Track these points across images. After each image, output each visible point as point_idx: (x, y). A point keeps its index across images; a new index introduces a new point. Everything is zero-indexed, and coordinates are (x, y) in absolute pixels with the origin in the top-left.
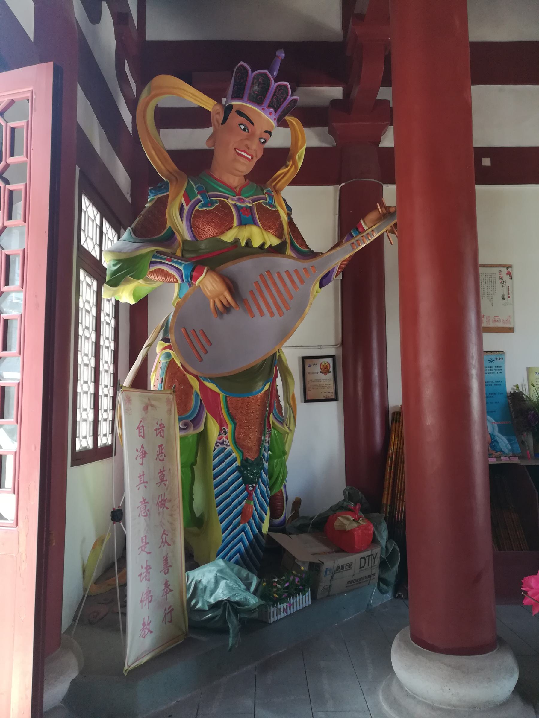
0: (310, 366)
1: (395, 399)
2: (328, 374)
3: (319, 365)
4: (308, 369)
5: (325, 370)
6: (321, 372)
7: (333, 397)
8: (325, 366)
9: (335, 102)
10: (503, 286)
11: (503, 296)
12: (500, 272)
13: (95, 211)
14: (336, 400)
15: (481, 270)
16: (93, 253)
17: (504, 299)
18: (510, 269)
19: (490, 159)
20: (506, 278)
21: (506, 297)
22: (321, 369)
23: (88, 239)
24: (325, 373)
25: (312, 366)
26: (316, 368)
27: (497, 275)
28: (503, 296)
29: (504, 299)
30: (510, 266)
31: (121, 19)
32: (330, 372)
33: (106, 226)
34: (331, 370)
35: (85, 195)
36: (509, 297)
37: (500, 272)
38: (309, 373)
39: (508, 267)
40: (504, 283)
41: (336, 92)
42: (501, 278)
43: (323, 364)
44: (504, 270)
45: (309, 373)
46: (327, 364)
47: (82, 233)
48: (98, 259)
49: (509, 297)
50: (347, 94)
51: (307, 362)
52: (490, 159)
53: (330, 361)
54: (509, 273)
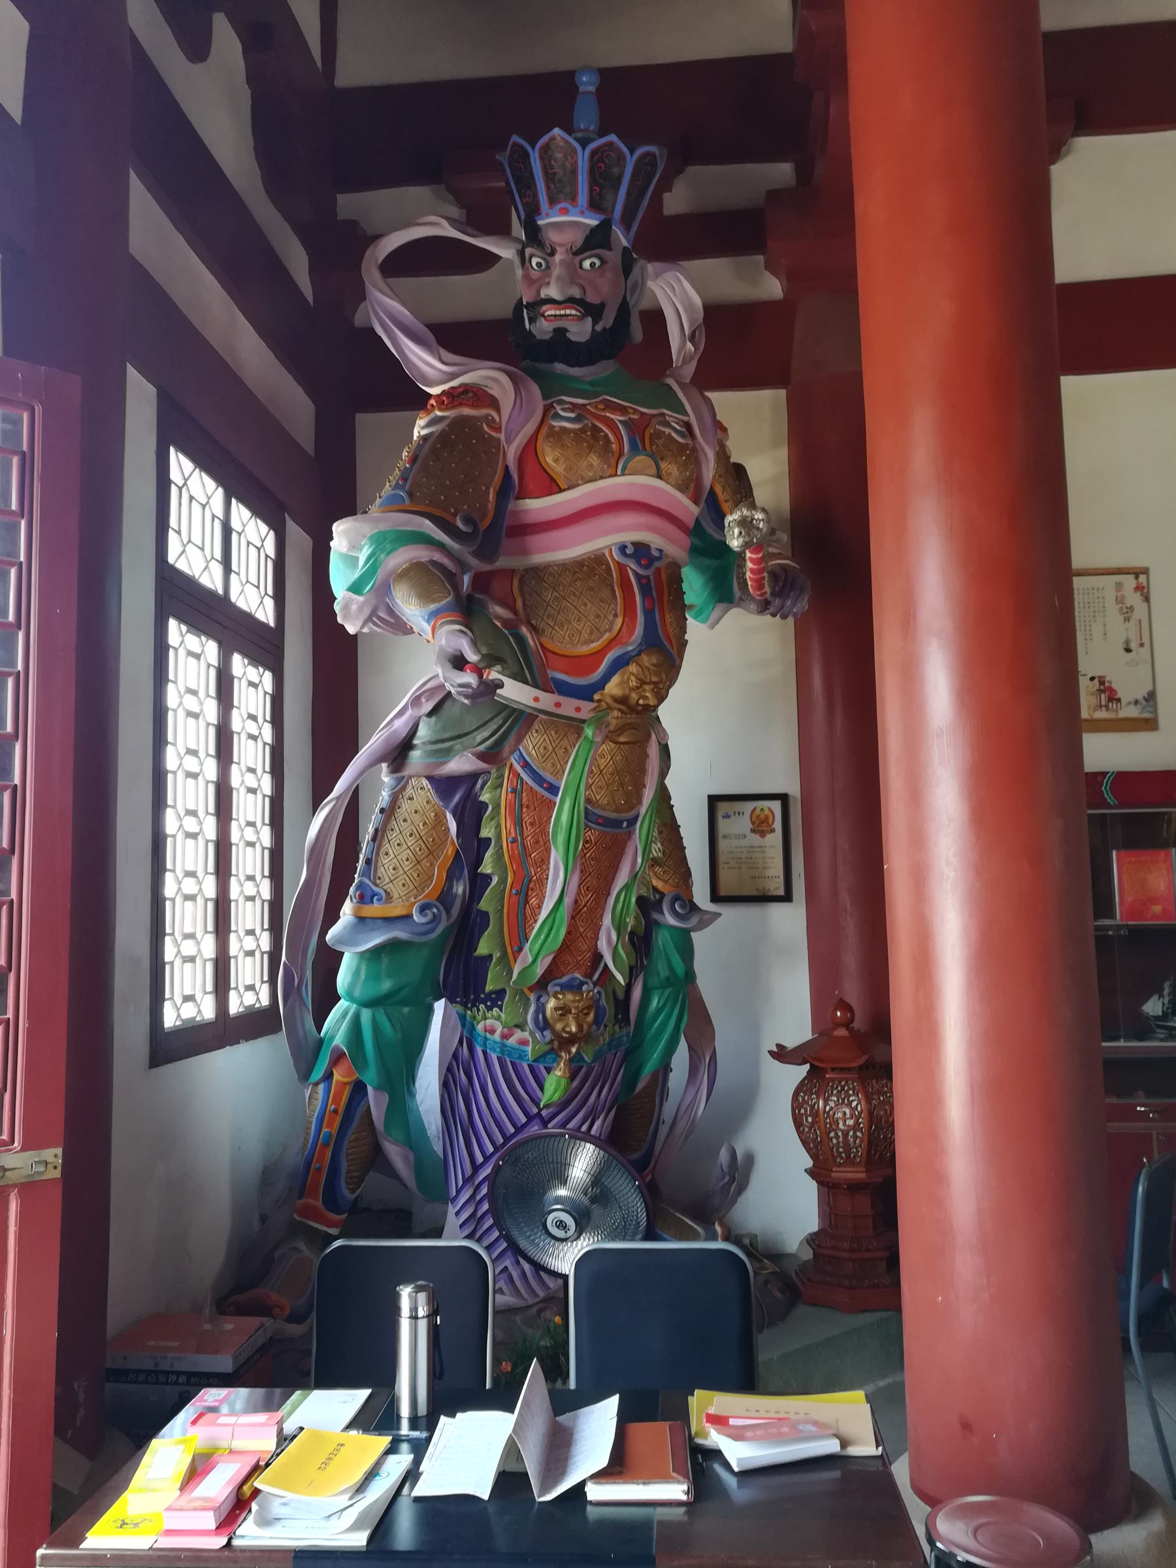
0: (727, 816)
1: (1165, 835)
2: (769, 837)
3: (747, 815)
4: (723, 826)
5: (761, 826)
6: (753, 831)
7: (781, 892)
8: (762, 817)
9: (774, 195)
10: (1127, 619)
11: (1127, 642)
12: (1119, 586)
13: (210, 484)
14: (787, 898)
15: (1077, 582)
16: (205, 581)
17: (1128, 650)
18: (1142, 578)
19: (1062, 378)
20: (1134, 599)
21: (1133, 646)
22: (753, 823)
23: (190, 547)
24: (763, 834)
25: (733, 817)
26: (736, 825)
27: (1110, 595)
28: (1127, 642)
29: (1128, 650)
30: (1146, 571)
31: (266, 36)
32: (773, 831)
33: (240, 514)
34: (778, 825)
35: (182, 449)
36: (1142, 645)
37: (1119, 586)
38: (725, 837)
39: (1137, 573)
40: (1127, 613)
41: (782, 172)
42: (1120, 600)
43: (758, 812)
44: (1129, 581)
45: (725, 837)
46: (767, 812)
47: (172, 535)
48: (220, 591)
49: (1142, 645)
50: (804, 174)
51: (723, 808)
52: (1062, 378)
53: (776, 806)
54: (1139, 588)
